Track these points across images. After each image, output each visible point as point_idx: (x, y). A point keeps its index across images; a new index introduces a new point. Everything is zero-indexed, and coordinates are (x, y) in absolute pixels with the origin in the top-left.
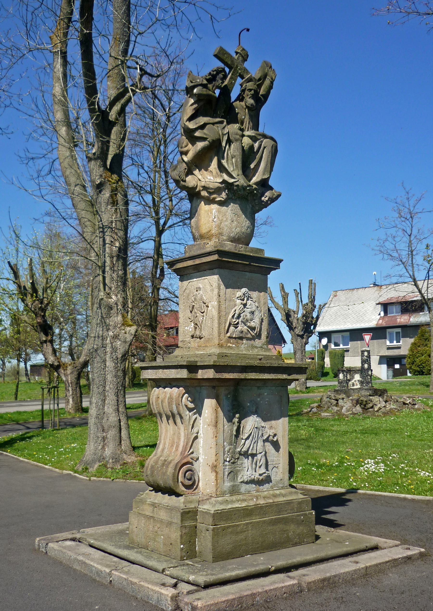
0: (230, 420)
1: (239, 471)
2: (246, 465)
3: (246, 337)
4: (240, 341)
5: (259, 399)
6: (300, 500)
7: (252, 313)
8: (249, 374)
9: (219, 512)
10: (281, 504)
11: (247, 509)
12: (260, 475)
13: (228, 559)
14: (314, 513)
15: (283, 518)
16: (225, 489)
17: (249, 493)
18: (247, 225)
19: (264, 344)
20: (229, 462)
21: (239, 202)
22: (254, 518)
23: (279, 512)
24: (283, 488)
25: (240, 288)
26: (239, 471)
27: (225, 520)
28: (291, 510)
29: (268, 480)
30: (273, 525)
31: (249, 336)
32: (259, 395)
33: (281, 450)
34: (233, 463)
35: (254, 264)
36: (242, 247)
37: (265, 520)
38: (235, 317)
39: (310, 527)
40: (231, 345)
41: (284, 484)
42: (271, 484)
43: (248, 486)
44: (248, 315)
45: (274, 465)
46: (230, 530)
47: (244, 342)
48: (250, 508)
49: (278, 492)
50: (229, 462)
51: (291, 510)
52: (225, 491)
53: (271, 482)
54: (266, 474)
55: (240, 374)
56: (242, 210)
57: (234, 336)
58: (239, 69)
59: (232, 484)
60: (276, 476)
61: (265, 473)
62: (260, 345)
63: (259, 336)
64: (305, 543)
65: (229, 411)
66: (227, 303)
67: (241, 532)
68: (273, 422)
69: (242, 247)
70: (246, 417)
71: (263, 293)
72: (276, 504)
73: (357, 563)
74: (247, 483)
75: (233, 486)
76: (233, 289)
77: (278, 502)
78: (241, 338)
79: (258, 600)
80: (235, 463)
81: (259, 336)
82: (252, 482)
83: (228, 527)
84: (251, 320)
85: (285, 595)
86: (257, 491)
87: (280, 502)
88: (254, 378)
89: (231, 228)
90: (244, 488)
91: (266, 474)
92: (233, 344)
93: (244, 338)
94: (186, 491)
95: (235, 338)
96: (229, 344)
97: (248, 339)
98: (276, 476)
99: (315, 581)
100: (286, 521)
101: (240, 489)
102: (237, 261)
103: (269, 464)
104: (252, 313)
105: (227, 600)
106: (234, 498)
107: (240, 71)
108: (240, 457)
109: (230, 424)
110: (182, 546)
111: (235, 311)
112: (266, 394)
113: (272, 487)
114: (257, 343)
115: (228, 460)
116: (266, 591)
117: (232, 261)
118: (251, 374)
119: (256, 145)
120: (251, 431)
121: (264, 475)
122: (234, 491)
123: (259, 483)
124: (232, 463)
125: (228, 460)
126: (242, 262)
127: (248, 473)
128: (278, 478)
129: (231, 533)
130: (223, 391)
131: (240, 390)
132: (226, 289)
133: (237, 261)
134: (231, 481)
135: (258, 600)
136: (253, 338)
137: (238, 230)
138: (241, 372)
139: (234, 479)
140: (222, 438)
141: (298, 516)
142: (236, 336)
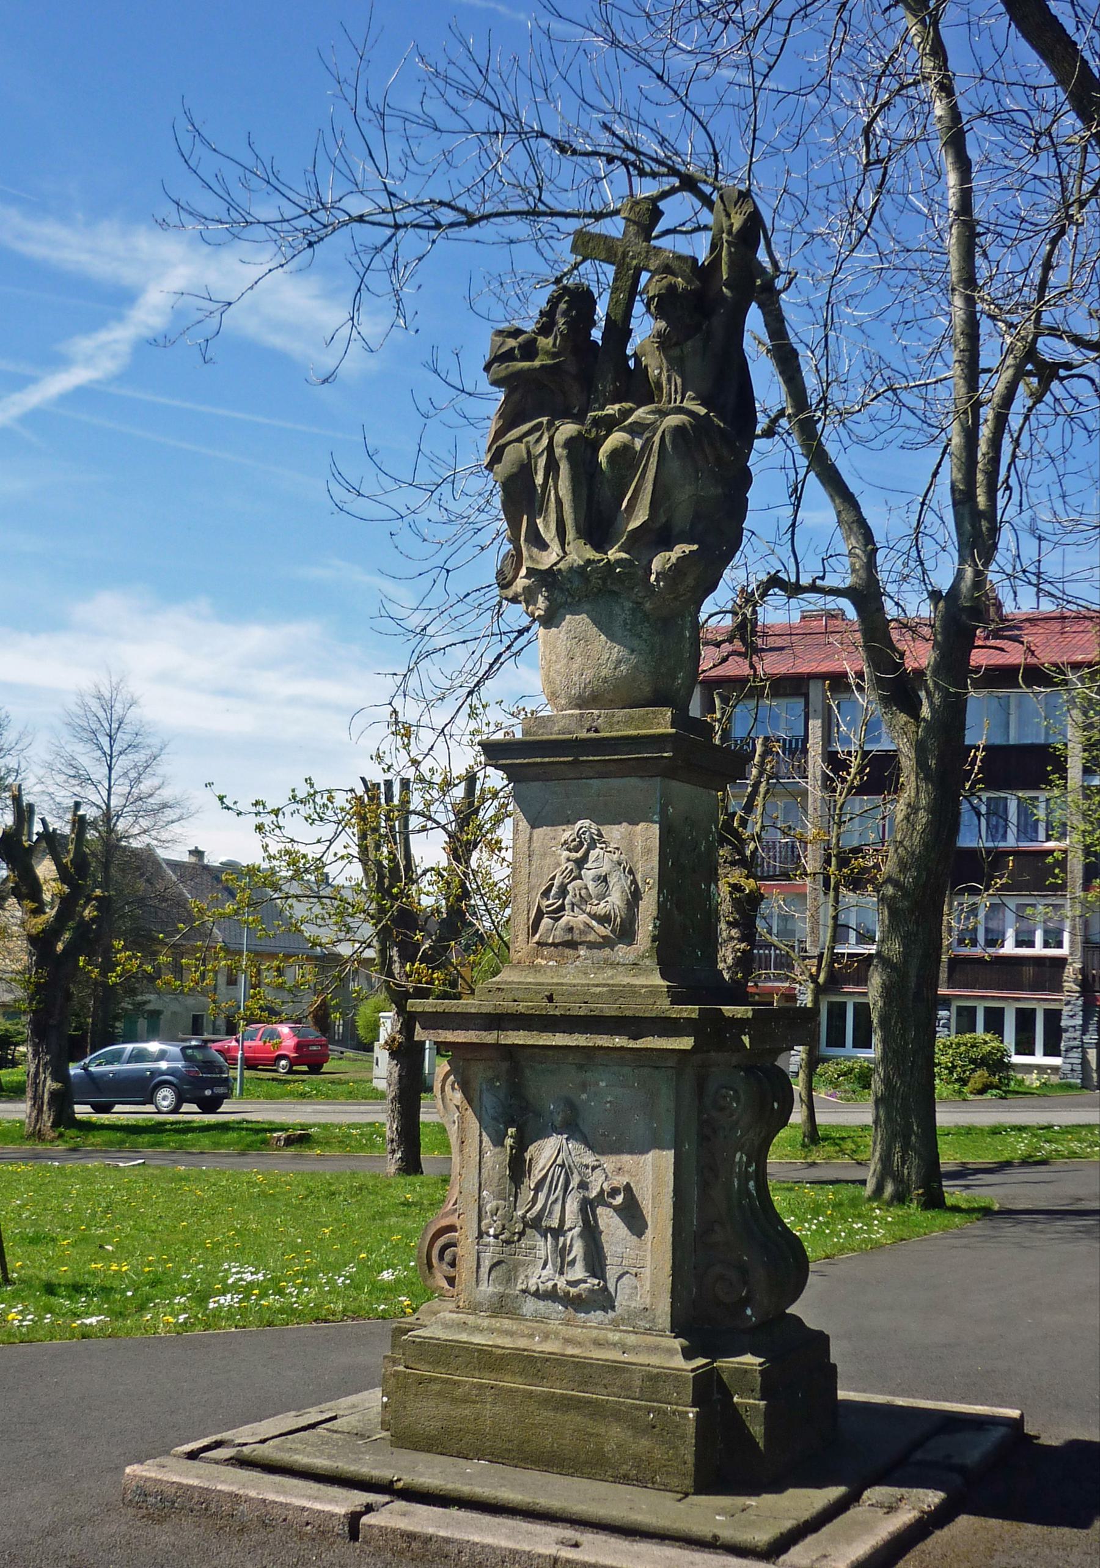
0: (498, 1142)
1: (523, 1264)
2: (543, 1252)
3: (585, 942)
4: (568, 952)
5: (584, 1096)
6: (656, 1371)
7: (604, 879)
8: (510, 1033)
9: (418, 1340)
10: (591, 1365)
11: (490, 1353)
12: (573, 1284)
13: (429, 1452)
14: (691, 1415)
15: (589, 1402)
16: (479, 1298)
17: (542, 1322)
18: (614, 657)
19: (643, 957)
20: (496, 1237)
21: (587, 607)
22: (507, 1378)
23: (584, 1384)
24: (648, 1331)
25: (570, 822)
26: (523, 1264)
27: (429, 1363)
28: (621, 1387)
29: (603, 1300)
30: (556, 1409)
31: (591, 937)
32: (584, 1087)
33: (649, 1232)
34: (508, 1242)
35: (591, 758)
36: (599, 716)
37: (532, 1392)
38: (553, 892)
39: (676, 1448)
40: (544, 962)
41: (653, 1321)
42: (611, 1314)
43: (541, 1304)
44: (591, 886)
45: (626, 1269)
46: (436, 1387)
47: (582, 953)
48: (500, 1351)
49: (632, 1339)
50: (496, 1237)
51: (621, 1387)
52: (481, 1304)
53: (613, 1308)
54: (587, 1285)
55: (484, 1033)
56: (596, 622)
57: (550, 941)
58: (633, 258)
59: (500, 1289)
60: (631, 1297)
61: (585, 1282)
62: (632, 958)
63: (626, 933)
64: (656, 1486)
65: (495, 1119)
66: (536, 862)
67: (465, 1401)
68: (626, 1158)
69: (599, 716)
70: (540, 1139)
71: (642, 825)
72: (573, 1362)
73: (576, 1545)
74: (537, 1295)
75: (502, 1296)
76: (553, 826)
77: (585, 1358)
78: (572, 945)
79: (243, 1511)
80: (513, 1242)
81: (626, 933)
82: (551, 1295)
83: (431, 1380)
84: (602, 897)
85: (309, 1527)
86: (567, 1323)
87: (591, 1359)
88: (521, 1043)
89: (568, 676)
90: (530, 1306)
91: (587, 1285)
92: (551, 959)
93: (581, 943)
94: (448, 1291)
95: (555, 945)
96: (539, 960)
97: (591, 946)
98: (631, 1297)
99: (386, 1528)
100: (596, 1410)
101: (520, 1307)
102: (539, 760)
103: (608, 1262)
104: (604, 879)
105: (179, 1484)
106: (496, 1323)
107: (635, 262)
108: (528, 1230)
109: (498, 1149)
110: (385, 1399)
111: (553, 878)
112: (602, 1084)
113: (613, 1322)
114: (622, 952)
115: (492, 1231)
116: (264, 1501)
117: (526, 761)
118: (515, 1033)
119: (638, 443)
120: (544, 1172)
121: (583, 1286)
122: (502, 1307)
123: (577, 1303)
124: (503, 1242)
125: (492, 1231)
126: (552, 759)
127: (545, 1273)
128: (636, 1304)
129: (439, 1394)
130: (479, 1072)
131: (528, 1072)
132: (533, 827)
133: (539, 760)
134: (499, 1284)
135: (243, 1511)
136: (606, 943)
137: (589, 674)
138: (488, 1028)
139: (510, 1279)
140: (476, 1180)
141: (638, 1408)
142: (557, 941)
